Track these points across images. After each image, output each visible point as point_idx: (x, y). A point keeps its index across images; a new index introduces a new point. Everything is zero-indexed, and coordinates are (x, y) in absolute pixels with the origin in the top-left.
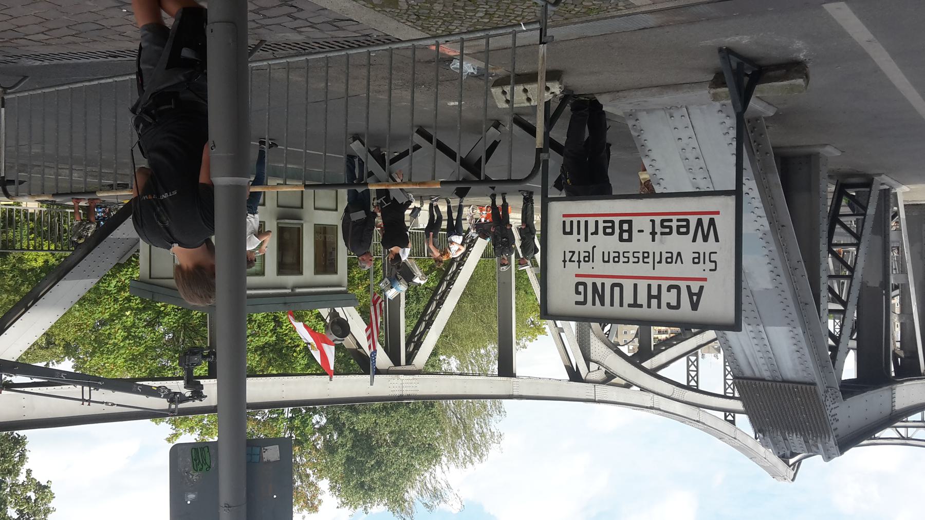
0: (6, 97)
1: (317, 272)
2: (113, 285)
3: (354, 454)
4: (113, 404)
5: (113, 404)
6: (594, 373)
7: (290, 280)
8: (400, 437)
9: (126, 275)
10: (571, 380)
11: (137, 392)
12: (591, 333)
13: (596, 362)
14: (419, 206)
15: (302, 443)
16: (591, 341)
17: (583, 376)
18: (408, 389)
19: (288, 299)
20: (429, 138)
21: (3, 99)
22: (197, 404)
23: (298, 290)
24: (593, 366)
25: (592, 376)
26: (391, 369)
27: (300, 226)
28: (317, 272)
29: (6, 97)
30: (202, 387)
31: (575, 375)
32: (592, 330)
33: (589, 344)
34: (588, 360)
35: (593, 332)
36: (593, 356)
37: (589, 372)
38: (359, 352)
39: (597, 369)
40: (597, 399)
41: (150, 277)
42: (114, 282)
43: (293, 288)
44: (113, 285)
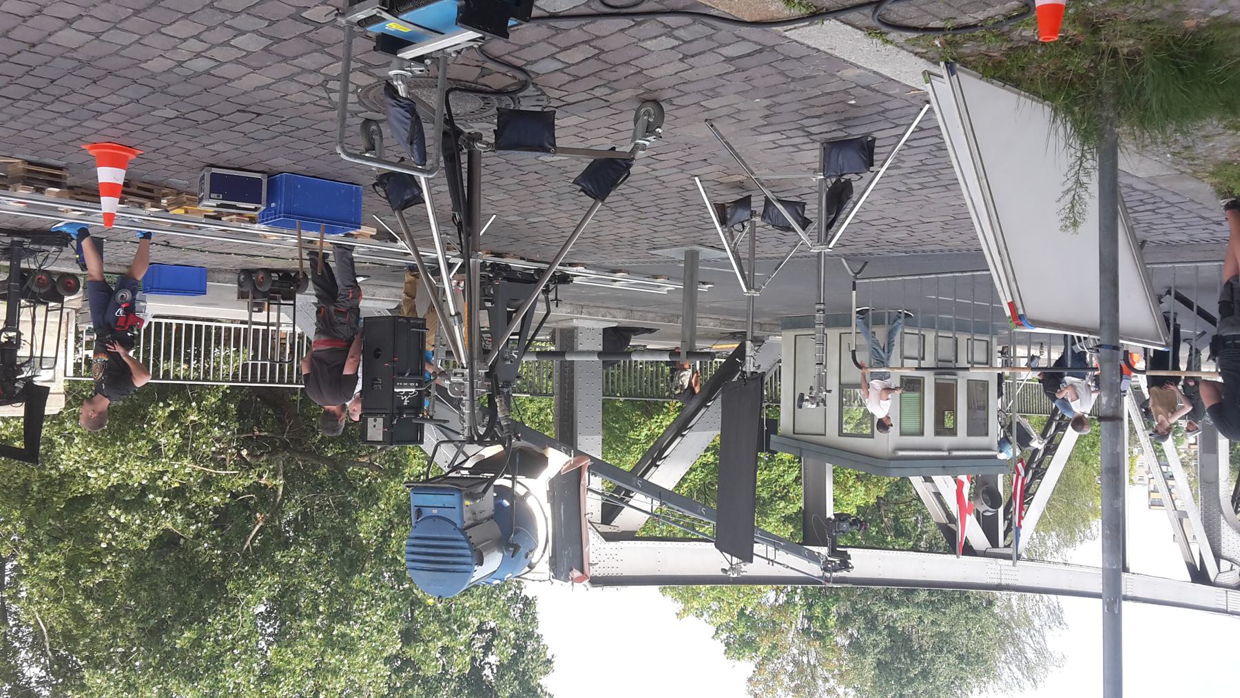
0: (857, 281)
1: (969, 434)
2: (643, 434)
3: (888, 659)
4: (788, 567)
5: (788, 567)
6: (1226, 574)
7: (946, 441)
8: (943, 642)
9: (656, 422)
10: (1193, 581)
11: (804, 557)
12: (1223, 521)
13: (1230, 560)
14: (1038, 354)
15: (823, 637)
16: (1222, 531)
17: (1212, 578)
18: (1007, 577)
19: (946, 463)
20: (1188, 304)
21: (854, 283)
22: (844, 574)
23: (901, 453)
24: (1225, 565)
25: (1222, 579)
26: (988, 550)
27: (954, 382)
28: (969, 434)
29: (857, 281)
30: (849, 557)
31: (1199, 575)
32: (1224, 516)
33: (1220, 535)
34: (1218, 557)
35: (1225, 518)
36: (1225, 551)
37: (1220, 572)
38: (949, 527)
39: (1229, 569)
40: (1229, 610)
41: (794, 433)
42: (645, 431)
43: (950, 450)
44: (643, 434)
